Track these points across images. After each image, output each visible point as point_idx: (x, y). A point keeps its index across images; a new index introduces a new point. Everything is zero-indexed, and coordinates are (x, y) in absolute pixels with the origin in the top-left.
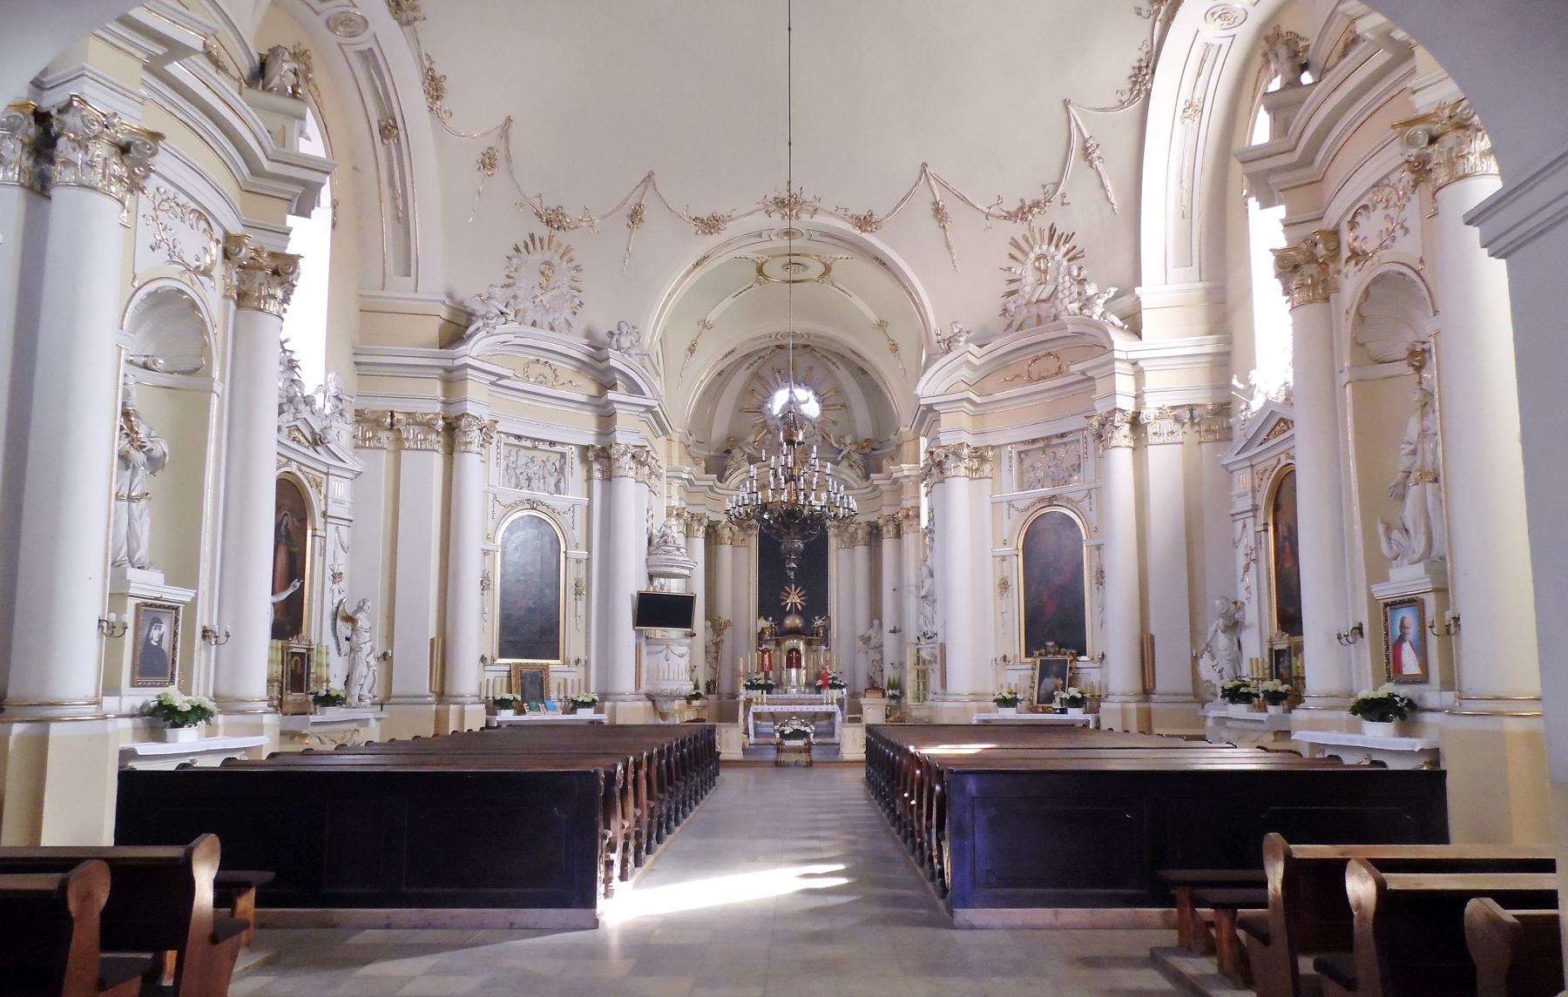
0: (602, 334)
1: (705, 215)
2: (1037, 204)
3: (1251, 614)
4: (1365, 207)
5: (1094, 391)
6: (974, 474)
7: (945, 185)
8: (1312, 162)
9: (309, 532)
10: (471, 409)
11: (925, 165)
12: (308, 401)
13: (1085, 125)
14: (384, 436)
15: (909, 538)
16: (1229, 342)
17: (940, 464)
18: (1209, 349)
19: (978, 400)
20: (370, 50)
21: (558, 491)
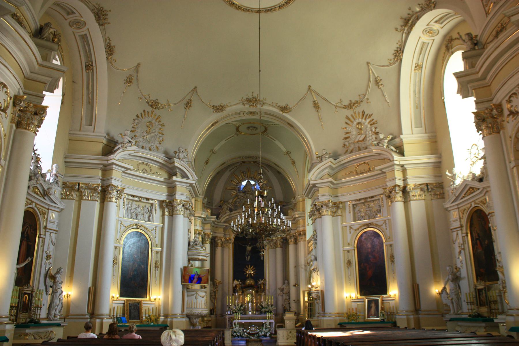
0: (172, 153)
1: (217, 104)
3: (464, 273)
4: (515, 94)
5: (386, 178)
7: (318, 94)
8: (485, 79)
9: (38, 236)
10: (114, 182)
11: (310, 86)
12: (44, 176)
14: (75, 194)
15: (301, 244)
16: (440, 157)
17: (318, 210)
18: (433, 160)
19: (335, 182)
20: (86, 35)
21: (149, 220)
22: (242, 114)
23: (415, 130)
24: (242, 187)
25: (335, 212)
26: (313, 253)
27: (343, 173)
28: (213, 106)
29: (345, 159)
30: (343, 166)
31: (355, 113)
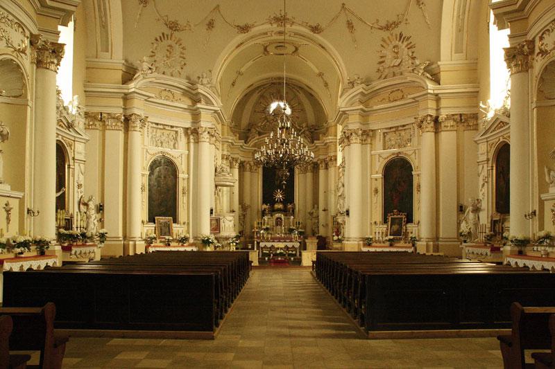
0: (194, 78)
3: (484, 205)
4: (548, 30)
6: (363, 142)
7: (353, 13)
9: (66, 166)
11: (343, 4)
15: (332, 170)
17: (348, 138)
21: (175, 148)
22: (269, 34)
23: (455, 56)
24: (271, 110)
25: (365, 140)
26: (342, 180)
27: (375, 100)
28: (238, 26)
29: (378, 84)
30: (375, 93)
31: (392, 35)
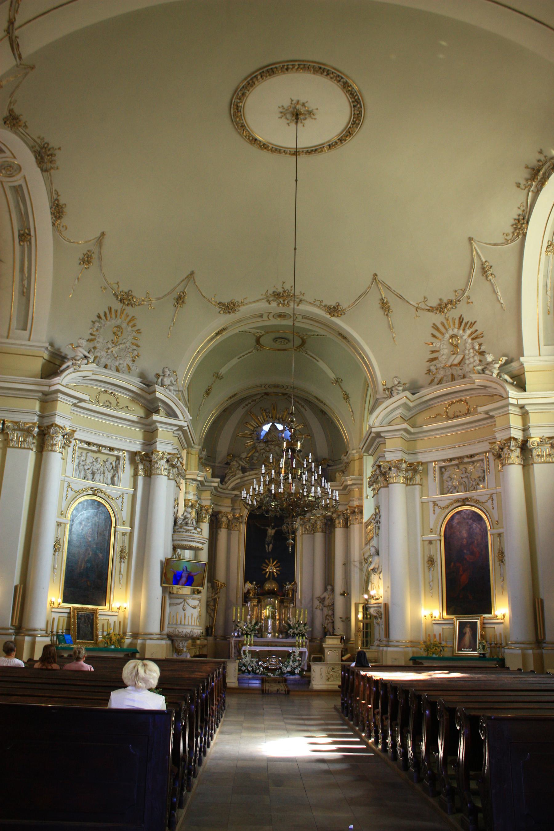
0: (151, 376)
1: (226, 301)
2: (451, 302)
6: (409, 481)
7: (389, 288)
10: (58, 421)
11: (375, 275)
13: (483, 254)
15: (355, 528)
17: (384, 474)
19: (412, 430)
20: (20, 186)
21: (113, 483)
22: (265, 317)
25: (411, 479)
26: (374, 543)
27: (426, 416)
28: (220, 303)
29: (428, 393)
30: (426, 405)
